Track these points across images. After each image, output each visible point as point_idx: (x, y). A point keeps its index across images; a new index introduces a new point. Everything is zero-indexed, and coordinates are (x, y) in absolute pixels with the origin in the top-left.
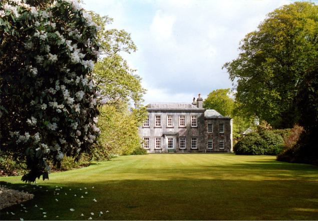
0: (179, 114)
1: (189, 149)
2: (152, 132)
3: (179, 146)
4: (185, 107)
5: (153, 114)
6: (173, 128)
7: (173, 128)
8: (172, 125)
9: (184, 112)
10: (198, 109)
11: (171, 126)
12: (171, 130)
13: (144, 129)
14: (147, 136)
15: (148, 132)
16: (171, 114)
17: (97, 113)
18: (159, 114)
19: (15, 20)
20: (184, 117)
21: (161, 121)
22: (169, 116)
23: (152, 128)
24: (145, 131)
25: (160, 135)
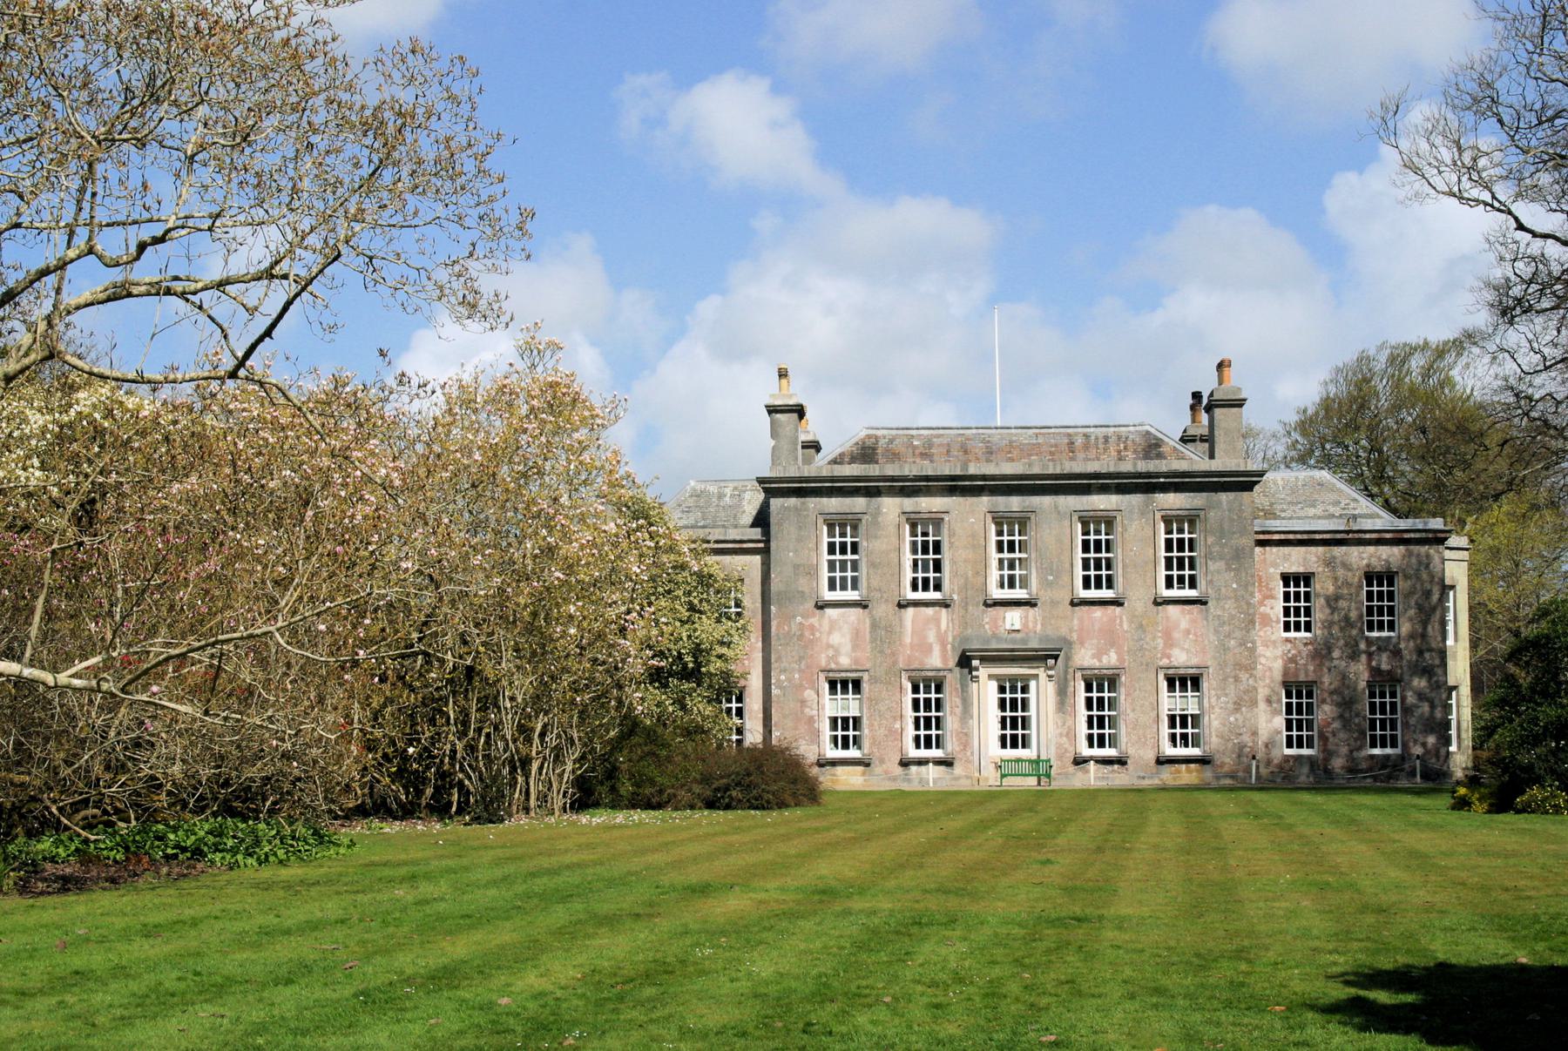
0: (774, 624)
1: (1150, 756)
2: (883, 635)
3: (1072, 735)
4: (1223, 425)
5: (891, 507)
6: (1030, 603)
7: (1030, 603)
8: (1024, 583)
9: (1104, 489)
10: (1215, 465)
11: (1018, 593)
12: (1013, 618)
13: (829, 612)
14: (845, 661)
15: (856, 635)
16: (1015, 503)
17: (546, 600)
18: (928, 504)
19: (957, 881)
20: (1110, 523)
21: (946, 556)
22: (1000, 520)
23: (883, 610)
24: (833, 626)
25: (937, 659)
